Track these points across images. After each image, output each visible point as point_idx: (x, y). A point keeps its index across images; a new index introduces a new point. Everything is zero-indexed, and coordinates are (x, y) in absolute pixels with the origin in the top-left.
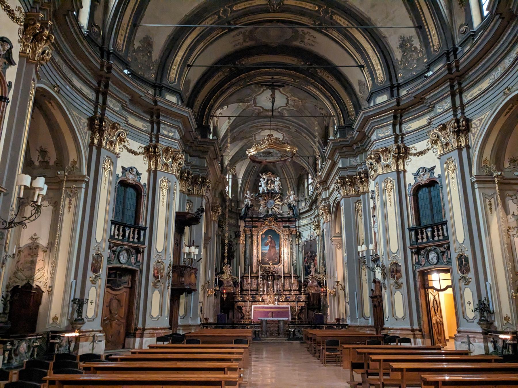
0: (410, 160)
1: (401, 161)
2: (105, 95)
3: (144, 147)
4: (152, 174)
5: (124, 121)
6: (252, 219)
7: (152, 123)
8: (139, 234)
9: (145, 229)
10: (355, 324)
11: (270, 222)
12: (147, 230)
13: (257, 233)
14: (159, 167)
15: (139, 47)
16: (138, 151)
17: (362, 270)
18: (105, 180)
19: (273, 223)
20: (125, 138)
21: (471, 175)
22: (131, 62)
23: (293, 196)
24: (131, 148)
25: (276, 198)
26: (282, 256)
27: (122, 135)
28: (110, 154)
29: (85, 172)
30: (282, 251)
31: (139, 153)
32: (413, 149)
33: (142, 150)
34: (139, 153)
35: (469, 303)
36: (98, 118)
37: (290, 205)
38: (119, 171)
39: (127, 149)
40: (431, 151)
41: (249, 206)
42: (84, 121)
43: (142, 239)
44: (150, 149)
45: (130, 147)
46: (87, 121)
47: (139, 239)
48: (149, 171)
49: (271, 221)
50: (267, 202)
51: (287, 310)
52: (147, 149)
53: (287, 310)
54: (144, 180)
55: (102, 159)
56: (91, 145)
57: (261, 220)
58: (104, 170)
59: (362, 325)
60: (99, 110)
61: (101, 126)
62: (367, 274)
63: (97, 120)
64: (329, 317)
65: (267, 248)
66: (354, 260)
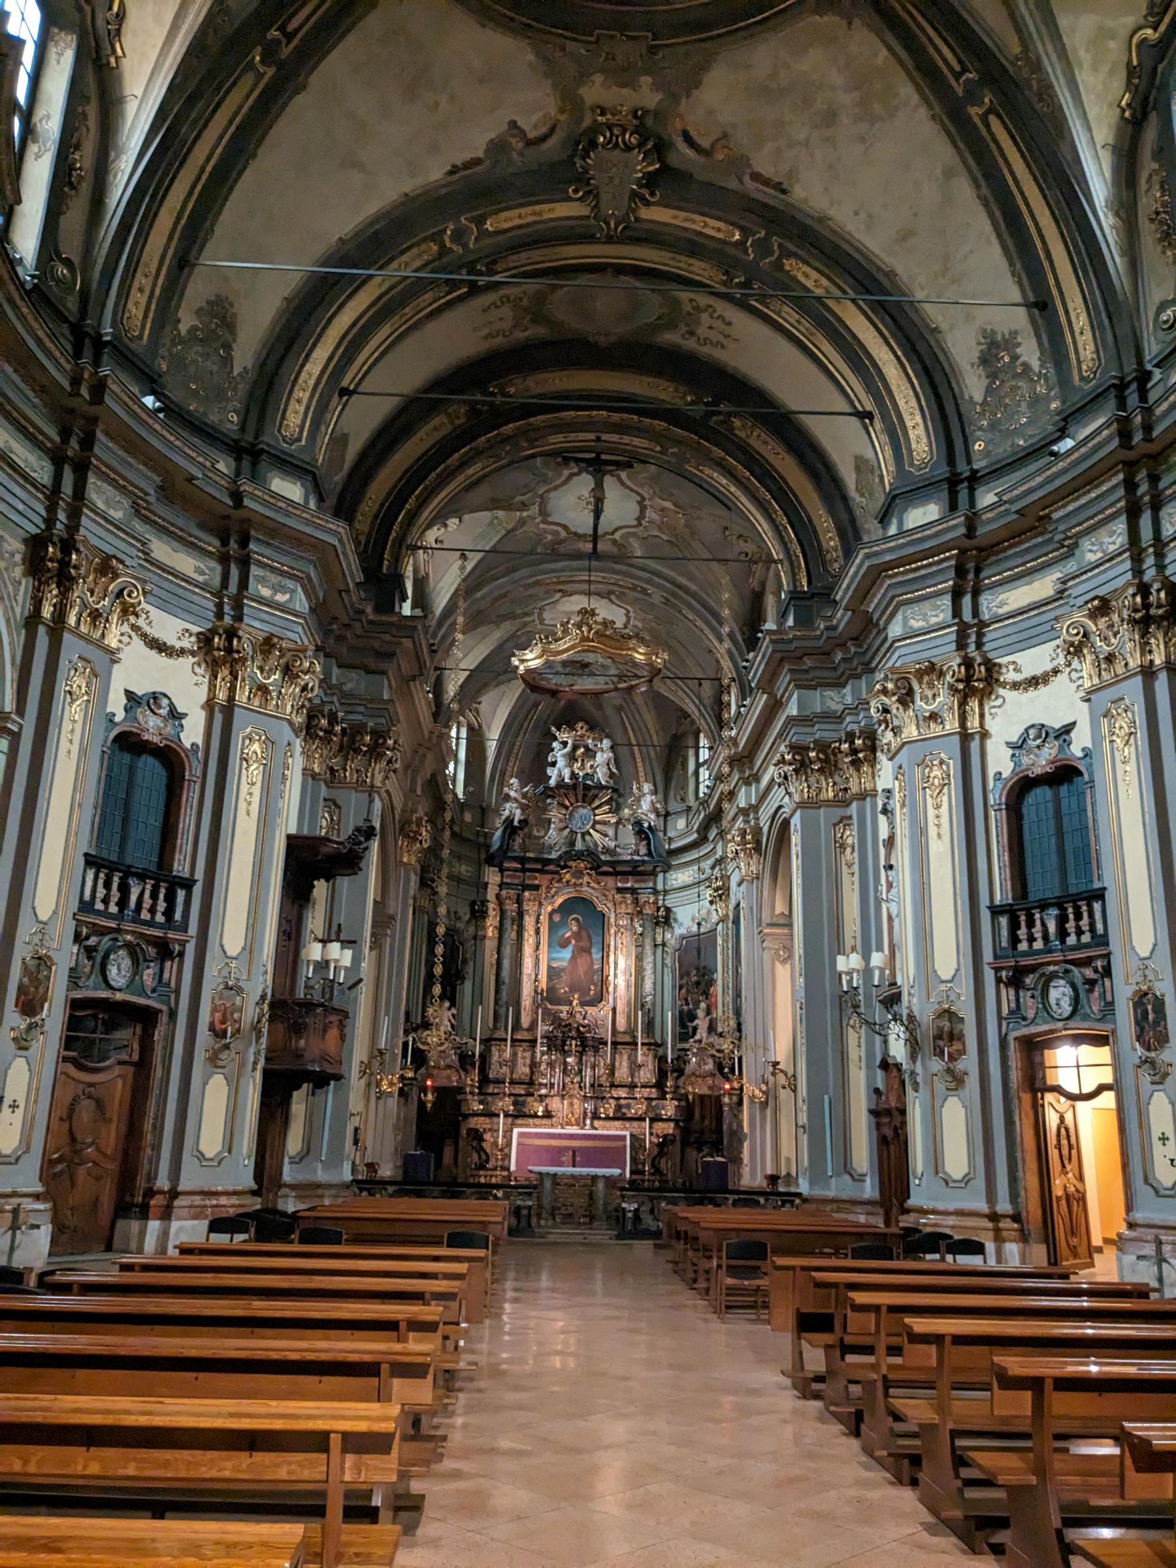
1: (974, 704)
4: (218, 718)
6: (523, 864)
7: (224, 560)
8: (170, 899)
9: (188, 884)
10: (823, 1193)
11: (578, 874)
13: (536, 908)
16: (178, 645)
17: (850, 1030)
19: (586, 879)
20: (140, 603)
23: (648, 798)
25: (597, 803)
26: (611, 978)
30: (612, 965)
31: (182, 652)
32: (1011, 667)
33: (188, 643)
34: (182, 652)
37: (641, 825)
38: (116, 705)
39: (144, 636)
40: (1062, 678)
41: (516, 823)
43: (178, 916)
44: (216, 640)
45: (154, 632)
47: (169, 913)
48: (209, 705)
49: (581, 872)
50: (571, 814)
51: (619, 1144)
52: (205, 640)
53: (619, 1144)
54: (192, 733)
55: (64, 664)
57: (551, 867)
59: (844, 1196)
61: (64, 564)
62: (863, 1040)
64: (746, 1170)
65: (567, 954)
66: (825, 995)
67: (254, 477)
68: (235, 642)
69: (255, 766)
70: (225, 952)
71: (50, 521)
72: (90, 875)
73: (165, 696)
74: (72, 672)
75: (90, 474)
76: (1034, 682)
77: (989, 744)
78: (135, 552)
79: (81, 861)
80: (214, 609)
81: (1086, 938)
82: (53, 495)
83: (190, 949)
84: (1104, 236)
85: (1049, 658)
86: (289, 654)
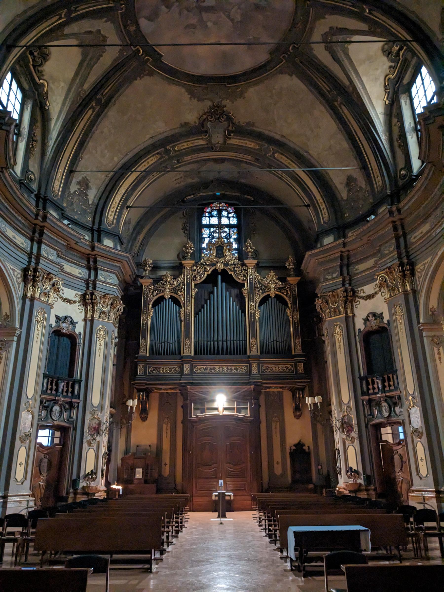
0: (358, 303)
1: (349, 304)
2: (40, 243)
3: (81, 295)
4: (88, 323)
5: (60, 269)
7: (89, 268)
8: (73, 387)
9: (80, 382)
12: (82, 383)
14: (96, 316)
15: (75, 192)
16: (74, 299)
18: (38, 334)
20: (60, 287)
21: (419, 322)
22: (67, 207)
24: (66, 297)
27: (57, 285)
28: (44, 306)
29: (17, 324)
31: (75, 302)
32: (362, 291)
33: (77, 299)
34: (75, 302)
35: (422, 460)
36: (31, 269)
38: (53, 321)
39: (62, 298)
40: (379, 295)
42: (18, 272)
43: (76, 392)
44: (87, 296)
45: (65, 296)
46: (20, 272)
47: (73, 392)
48: (85, 320)
52: (83, 297)
54: (79, 329)
55: (35, 311)
56: (24, 297)
58: (37, 323)
60: (33, 260)
61: (34, 276)
63: (31, 271)
67: (99, 240)
68: (94, 296)
69: (102, 339)
70: (93, 405)
71: (30, 262)
72: (46, 381)
73: (71, 318)
74: (38, 313)
75: (42, 244)
76: (369, 297)
77: (356, 319)
78: (57, 270)
79: (42, 376)
80: (85, 286)
81: (392, 388)
82: (30, 255)
83: (81, 404)
84: (384, 147)
85: (373, 289)
86: (112, 299)
